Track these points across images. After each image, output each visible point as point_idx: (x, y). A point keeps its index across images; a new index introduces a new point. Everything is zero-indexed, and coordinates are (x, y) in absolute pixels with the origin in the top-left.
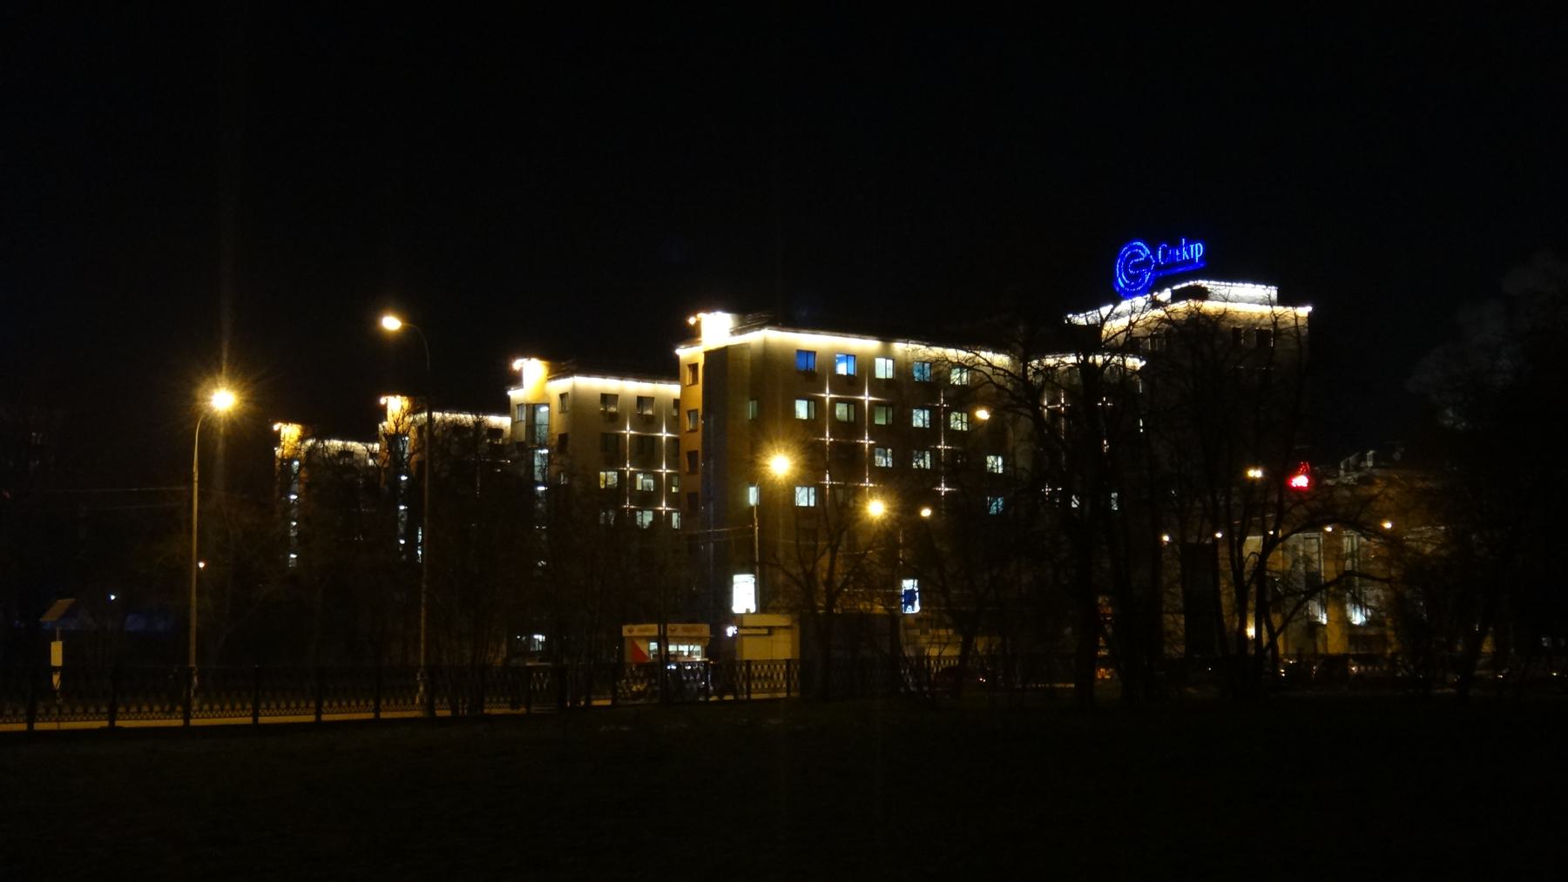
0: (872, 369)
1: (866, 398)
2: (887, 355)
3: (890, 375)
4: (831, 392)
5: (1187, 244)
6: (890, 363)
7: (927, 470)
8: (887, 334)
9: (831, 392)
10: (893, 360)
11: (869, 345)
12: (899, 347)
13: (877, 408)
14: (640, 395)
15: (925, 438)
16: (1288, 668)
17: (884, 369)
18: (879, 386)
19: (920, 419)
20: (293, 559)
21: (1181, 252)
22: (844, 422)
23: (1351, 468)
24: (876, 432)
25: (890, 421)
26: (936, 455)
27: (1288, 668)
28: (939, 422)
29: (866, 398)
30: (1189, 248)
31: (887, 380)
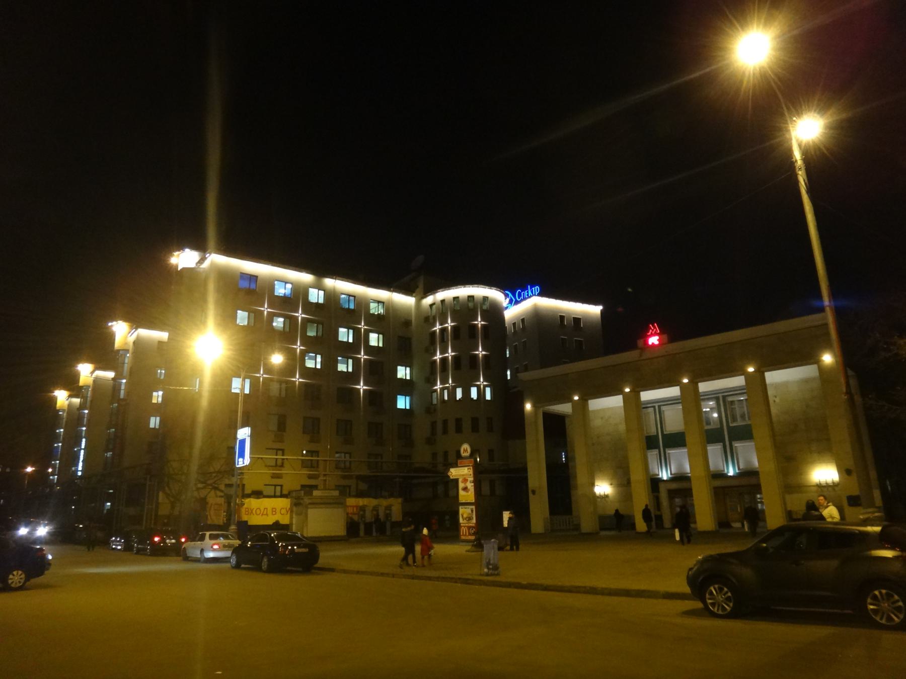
0: (306, 294)
1: (300, 315)
2: (319, 287)
3: (321, 301)
4: (269, 307)
5: (531, 288)
6: (322, 293)
7: (350, 372)
8: (321, 270)
9: (269, 307)
10: (324, 291)
11: (306, 278)
12: (329, 282)
13: (309, 324)
14: (160, 340)
15: (348, 350)
16: (41, 476)
17: (316, 296)
18: (311, 308)
19: (345, 335)
20: (108, 505)
21: (528, 292)
22: (280, 331)
23: (496, 572)
24: (306, 341)
25: (320, 334)
26: (356, 362)
27: (41, 476)
28: (361, 339)
29: (300, 315)
30: (532, 290)
31: (317, 304)
